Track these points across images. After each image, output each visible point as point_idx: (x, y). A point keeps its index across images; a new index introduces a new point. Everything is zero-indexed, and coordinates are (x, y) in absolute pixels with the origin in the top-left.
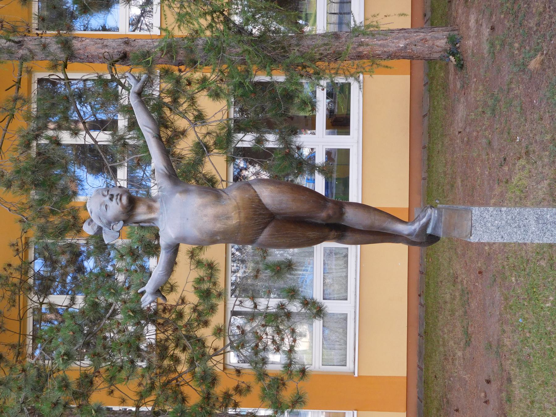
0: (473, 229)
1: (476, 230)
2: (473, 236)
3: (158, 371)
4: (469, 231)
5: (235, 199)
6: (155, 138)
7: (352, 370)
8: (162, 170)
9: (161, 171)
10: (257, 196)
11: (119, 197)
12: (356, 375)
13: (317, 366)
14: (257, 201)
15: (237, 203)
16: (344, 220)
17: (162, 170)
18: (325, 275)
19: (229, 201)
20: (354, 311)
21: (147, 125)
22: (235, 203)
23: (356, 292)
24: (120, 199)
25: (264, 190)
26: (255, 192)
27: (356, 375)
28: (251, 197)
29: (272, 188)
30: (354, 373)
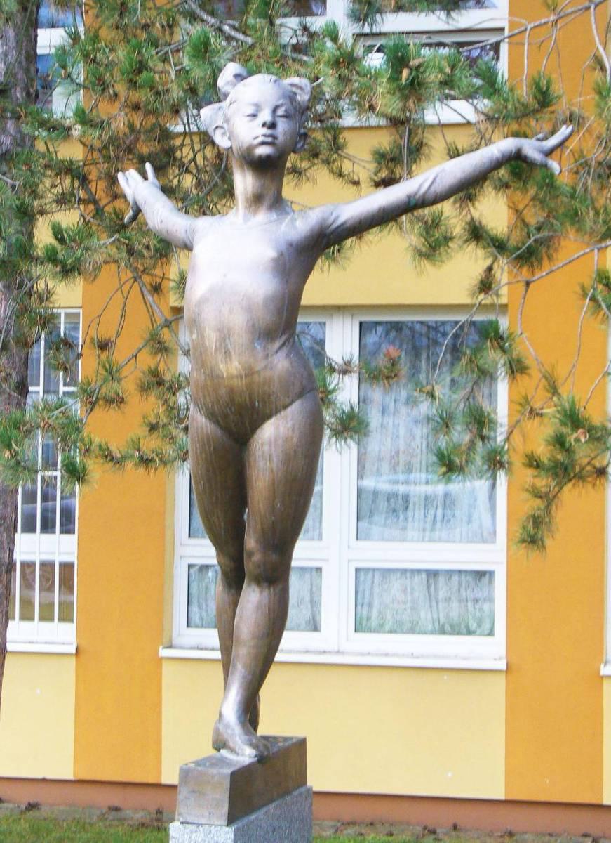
0: (194, 828)
1: (191, 832)
2: (181, 826)
3: (320, 108)
4: (189, 819)
5: (266, 367)
6: (407, 199)
7: (176, 641)
8: (337, 218)
9: (332, 218)
10: (277, 411)
11: (269, 139)
12: (164, 653)
13: (188, 551)
14: (268, 411)
15: (258, 372)
16: (249, 585)
17: (337, 218)
18: (455, 578)
19: (261, 355)
20: (327, 649)
21: (438, 180)
22: (257, 368)
23: (394, 655)
24: (263, 143)
25: (290, 424)
26: (285, 407)
27: (164, 653)
28: (273, 398)
29: (295, 440)
30: (170, 647)
